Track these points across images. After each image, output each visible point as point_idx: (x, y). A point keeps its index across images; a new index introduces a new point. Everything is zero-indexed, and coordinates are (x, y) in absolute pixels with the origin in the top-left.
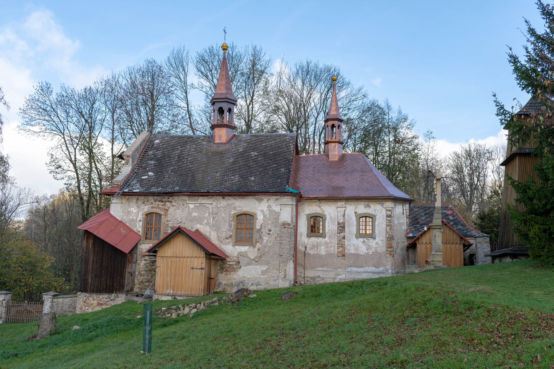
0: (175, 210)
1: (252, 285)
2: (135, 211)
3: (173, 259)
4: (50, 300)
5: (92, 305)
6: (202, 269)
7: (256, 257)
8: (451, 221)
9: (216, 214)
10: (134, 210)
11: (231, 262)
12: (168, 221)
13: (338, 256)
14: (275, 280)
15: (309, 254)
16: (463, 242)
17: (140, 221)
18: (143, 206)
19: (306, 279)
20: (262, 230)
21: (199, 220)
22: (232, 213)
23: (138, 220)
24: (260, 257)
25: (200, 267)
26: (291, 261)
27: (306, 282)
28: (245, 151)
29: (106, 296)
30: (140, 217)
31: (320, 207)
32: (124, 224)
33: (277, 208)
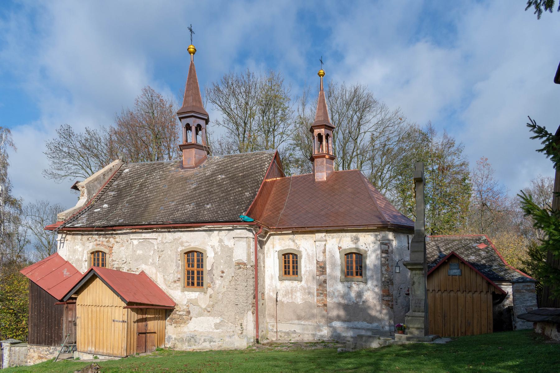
0: (120, 247)
1: (205, 341)
2: (80, 249)
3: (94, 309)
4: (8, 348)
5: (33, 357)
6: (123, 321)
7: (208, 306)
8: (483, 259)
9: (162, 251)
10: (79, 248)
11: (180, 310)
12: (113, 261)
13: (318, 306)
14: (230, 337)
15: (283, 303)
16: (492, 289)
17: (86, 261)
18: (87, 244)
19: (279, 334)
20: (214, 272)
21: (144, 259)
22: (179, 250)
23: (84, 260)
24: (213, 306)
25: (121, 320)
26: (250, 313)
27: (279, 338)
28: (212, 175)
29: (45, 348)
30: (86, 256)
31: (294, 241)
32: (70, 264)
33: (229, 243)
